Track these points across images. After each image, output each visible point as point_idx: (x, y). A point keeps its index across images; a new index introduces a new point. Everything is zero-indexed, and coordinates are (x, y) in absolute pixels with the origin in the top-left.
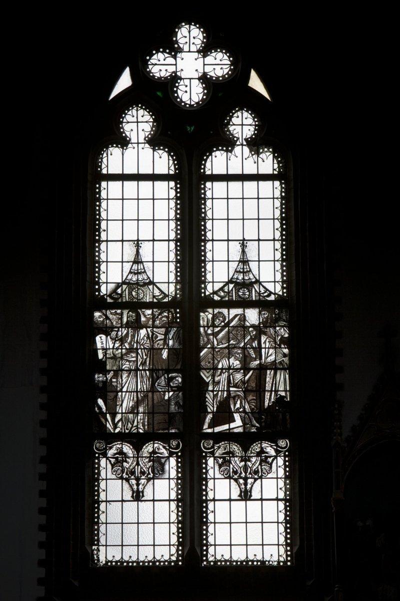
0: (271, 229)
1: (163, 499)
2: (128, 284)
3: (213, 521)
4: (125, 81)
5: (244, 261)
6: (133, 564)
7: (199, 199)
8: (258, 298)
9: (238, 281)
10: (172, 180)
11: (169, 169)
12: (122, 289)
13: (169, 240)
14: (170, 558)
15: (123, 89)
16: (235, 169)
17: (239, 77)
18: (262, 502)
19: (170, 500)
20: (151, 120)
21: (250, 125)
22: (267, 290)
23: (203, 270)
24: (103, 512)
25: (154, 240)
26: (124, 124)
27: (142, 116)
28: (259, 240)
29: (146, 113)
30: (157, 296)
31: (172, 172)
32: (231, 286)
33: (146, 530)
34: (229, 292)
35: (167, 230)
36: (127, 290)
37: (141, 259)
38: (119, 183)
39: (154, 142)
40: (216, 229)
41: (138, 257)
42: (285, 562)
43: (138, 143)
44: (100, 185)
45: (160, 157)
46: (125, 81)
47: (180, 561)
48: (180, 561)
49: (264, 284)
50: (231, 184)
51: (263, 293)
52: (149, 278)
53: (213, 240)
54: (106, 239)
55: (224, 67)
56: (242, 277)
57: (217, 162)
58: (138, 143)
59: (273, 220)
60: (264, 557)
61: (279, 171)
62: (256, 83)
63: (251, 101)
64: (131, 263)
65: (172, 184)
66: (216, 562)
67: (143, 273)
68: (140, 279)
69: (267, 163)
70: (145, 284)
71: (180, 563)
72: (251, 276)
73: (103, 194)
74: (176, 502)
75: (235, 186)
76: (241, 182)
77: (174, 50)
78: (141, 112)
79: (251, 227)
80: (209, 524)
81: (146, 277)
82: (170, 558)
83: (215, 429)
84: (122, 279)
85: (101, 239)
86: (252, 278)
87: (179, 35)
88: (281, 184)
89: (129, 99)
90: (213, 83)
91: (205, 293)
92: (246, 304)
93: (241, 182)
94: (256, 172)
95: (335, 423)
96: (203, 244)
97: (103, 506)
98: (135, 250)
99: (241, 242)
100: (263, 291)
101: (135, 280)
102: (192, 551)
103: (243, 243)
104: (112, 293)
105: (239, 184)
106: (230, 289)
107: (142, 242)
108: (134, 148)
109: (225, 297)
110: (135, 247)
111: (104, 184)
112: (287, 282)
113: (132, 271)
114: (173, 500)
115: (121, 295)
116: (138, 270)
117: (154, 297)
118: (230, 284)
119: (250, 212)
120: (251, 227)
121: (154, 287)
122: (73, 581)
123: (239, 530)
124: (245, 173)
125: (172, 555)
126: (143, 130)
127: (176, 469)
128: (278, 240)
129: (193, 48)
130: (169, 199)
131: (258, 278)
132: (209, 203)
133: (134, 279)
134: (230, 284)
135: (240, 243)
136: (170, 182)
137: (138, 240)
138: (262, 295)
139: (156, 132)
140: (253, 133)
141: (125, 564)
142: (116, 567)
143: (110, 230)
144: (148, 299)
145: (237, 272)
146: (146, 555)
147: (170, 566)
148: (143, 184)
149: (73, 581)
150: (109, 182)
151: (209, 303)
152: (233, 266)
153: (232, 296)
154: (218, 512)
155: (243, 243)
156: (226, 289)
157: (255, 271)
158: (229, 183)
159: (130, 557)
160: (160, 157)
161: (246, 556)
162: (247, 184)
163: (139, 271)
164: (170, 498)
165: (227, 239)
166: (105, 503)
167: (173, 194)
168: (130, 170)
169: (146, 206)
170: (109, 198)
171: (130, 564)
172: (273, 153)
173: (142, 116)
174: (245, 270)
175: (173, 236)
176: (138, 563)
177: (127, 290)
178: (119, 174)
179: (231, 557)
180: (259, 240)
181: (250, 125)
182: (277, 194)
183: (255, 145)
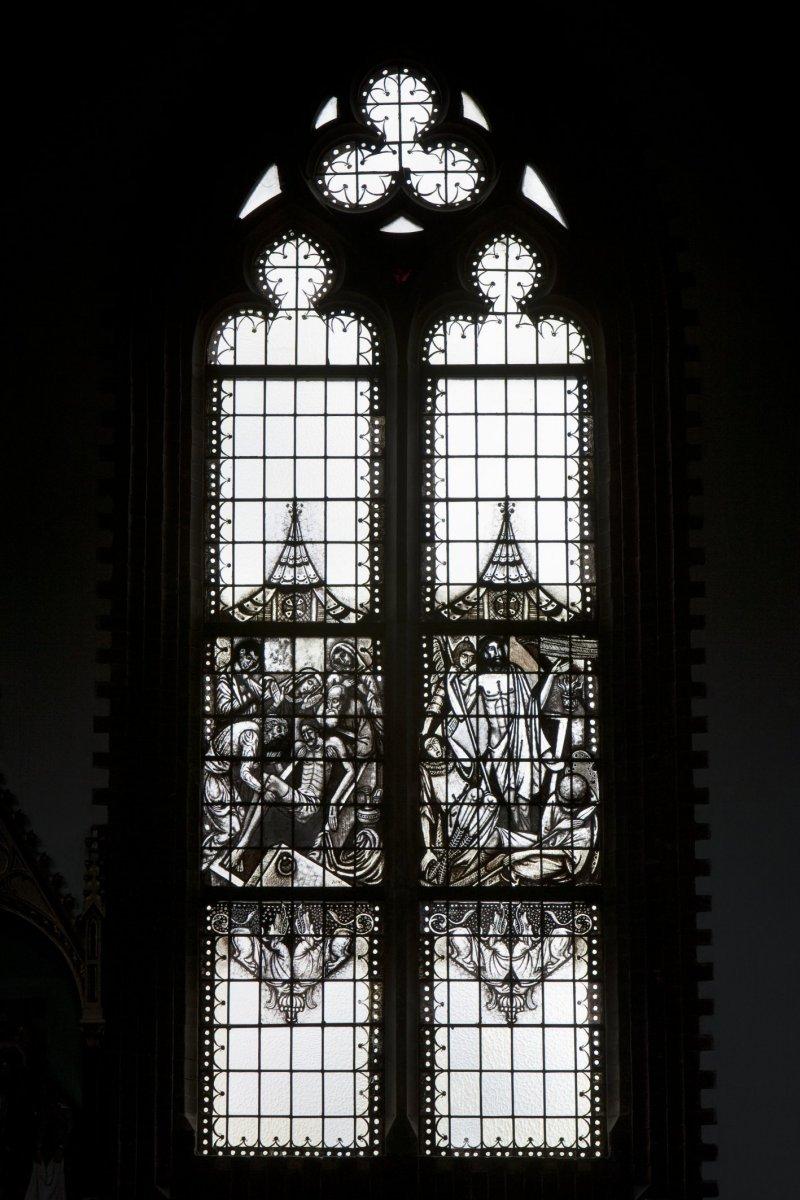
0: (560, 477)
1: (310, 1022)
2: (280, 589)
6: (535, 1154)
8: (321, 618)
9: (284, 583)
11: (569, 353)
12: (264, 597)
13: (233, 500)
14: (355, 1144)
15: (535, 201)
16: (491, 356)
18: (480, 1031)
20: (322, 264)
22: (552, 599)
23: (376, 558)
25: (537, 499)
26: (534, 268)
27: (518, 258)
28: (326, 499)
30: (332, 609)
31: (574, 360)
32: (271, 592)
33: (528, 1085)
34: (265, 605)
35: (352, 479)
37: (513, 535)
40: (452, 477)
41: (507, 527)
42: (590, 1150)
43: (297, 309)
46: (268, 187)
47: (597, 1149)
48: (597, 1149)
49: (545, 587)
50: (272, 385)
51: (546, 606)
53: (566, 499)
55: (360, 158)
56: (292, 574)
57: (453, 343)
58: (297, 309)
60: (325, 1140)
63: (527, 224)
64: (494, 544)
65: (364, 386)
66: (227, 1149)
67: (307, 564)
68: (513, 577)
69: (561, 342)
70: (310, 588)
71: (598, 1154)
72: (523, 571)
74: (368, 1028)
75: (280, 389)
76: (232, 382)
78: (304, 248)
80: (589, 1068)
81: (311, 572)
83: (537, 873)
85: (221, 497)
86: (524, 575)
89: (277, 223)
92: (294, 630)
93: (533, 381)
94: (533, 361)
96: (428, 507)
97: (441, 1036)
98: (500, 516)
99: (503, 502)
100: (544, 603)
101: (290, 578)
102: (402, 1126)
103: (506, 503)
104: (245, 600)
105: (528, 384)
106: (481, 594)
107: (305, 504)
110: (502, 512)
111: (227, 385)
116: (295, 558)
117: (327, 612)
118: (267, 590)
120: (310, 472)
122: (160, 1189)
123: (276, 1085)
124: (542, 361)
125: (581, 1139)
126: (519, 284)
128: (573, 499)
131: (322, 575)
132: (440, 423)
133: (500, 576)
135: (500, 505)
136: (359, 383)
137: (507, 499)
138: (332, 612)
139: (331, 288)
141: (233, 1153)
142: (566, 1161)
143: (238, 478)
145: (282, 564)
147: (355, 1159)
150: (268, 383)
152: (273, 551)
153: (271, 612)
154: (455, 1049)
155: (295, 510)
159: (530, 1140)
163: (298, 562)
166: (446, 1029)
167: (573, 403)
168: (281, 357)
169: (310, 429)
170: (262, 418)
171: (308, 1154)
172: (357, 318)
173: (518, 258)
174: (511, 560)
175: (364, 490)
176: (546, 1150)
178: (562, 365)
179: (259, 1141)
180: (537, 499)
182: (364, 405)
183: (536, 307)
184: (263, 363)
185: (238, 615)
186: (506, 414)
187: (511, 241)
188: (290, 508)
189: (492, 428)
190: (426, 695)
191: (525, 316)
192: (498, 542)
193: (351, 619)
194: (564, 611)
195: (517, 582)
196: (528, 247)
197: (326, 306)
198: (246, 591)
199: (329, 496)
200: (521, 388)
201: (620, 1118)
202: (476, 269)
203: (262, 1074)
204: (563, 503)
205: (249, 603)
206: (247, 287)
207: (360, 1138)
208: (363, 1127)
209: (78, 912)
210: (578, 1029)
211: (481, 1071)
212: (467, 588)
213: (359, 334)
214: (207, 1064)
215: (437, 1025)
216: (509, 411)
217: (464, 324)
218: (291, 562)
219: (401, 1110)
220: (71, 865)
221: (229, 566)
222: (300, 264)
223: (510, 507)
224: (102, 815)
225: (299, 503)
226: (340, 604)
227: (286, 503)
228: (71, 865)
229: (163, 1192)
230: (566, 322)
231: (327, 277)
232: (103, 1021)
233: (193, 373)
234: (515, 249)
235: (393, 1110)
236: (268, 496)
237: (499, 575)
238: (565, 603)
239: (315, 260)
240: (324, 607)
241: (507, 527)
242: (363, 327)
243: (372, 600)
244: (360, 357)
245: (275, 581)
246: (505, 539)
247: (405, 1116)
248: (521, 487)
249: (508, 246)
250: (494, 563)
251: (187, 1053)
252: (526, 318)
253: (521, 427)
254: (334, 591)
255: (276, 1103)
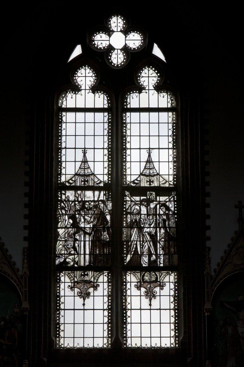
0: (166, 142)
2: (145, 175)
3: (130, 322)
4: (78, 51)
5: (85, 161)
7: (176, 123)
10: (170, 112)
14: (171, 346)
15: (157, 55)
17: (146, 49)
19: (64, 310)
21: (155, 77)
24: (129, 317)
27: (89, 73)
29: (80, 71)
33: (89, 328)
34: (75, 181)
35: (102, 142)
36: (78, 179)
37: (152, 160)
38: (138, 114)
39: (159, 88)
40: (133, 142)
43: (85, 90)
44: (126, 115)
45: (99, 97)
46: (78, 51)
50: (78, 114)
52: (92, 172)
54: (169, 150)
57: (134, 100)
59: (150, 137)
61: (108, 106)
62: (157, 52)
63: (154, 63)
64: (81, 163)
65: (106, 114)
70: (89, 175)
72: (89, 171)
73: (128, 121)
75: (144, 115)
77: (109, 32)
79: (89, 140)
82: (103, 346)
84: (75, 173)
87: (112, 22)
88: (173, 114)
89: (80, 62)
90: (130, 52)
91: (60, 180)
95: (206, 261)
98: (147, 155)
99: (83, 150)
100: (96, 180)
104: (135, 180)
105: (73, 114)
108: (146, 93)
109: (138, 183)
112: (176, 177)
113: (81, 167)
114: (106, 310)
115: (75, 181)
119: (89, 131)
120: (89, 140)
121: (161, 176)
125: (172, 344)
127: (60, 289)
129: (119, 30)
130: (168, 123)
131: (158, 172)
133: (148, 172)
134: (76, 176)
137: (85, 148)
139: (96, 83)
140: (156, 82)
143: (67, 141)
144: (91, 184)
146: (156, 343)
148: (142, 114)
149: (43, 358)
150: (141, 113)
151: (64, 187)
154: (133, 316)
155: (85, 150)
156: (74, 179)
157: (157, 168)
158: (67, 113)
160: (99, 97)
161: (140, 345)
162: (87, 114)
164: (64, 308)
165: (76, 149)
168: (144, 105)
173: (89, 73)
177: (78, 179)
181: (155, 77)
182: (170, 120)
184: (138, 107)
185: (67, 184)
186: (149, 123)
187: (87, 68)
188: (148, 151)
189: (144, 127)
190: (124, 209)
191: (91, 90)
192: (147, 162)
193: (102, 185)
194: (167, 183)
195: (87, 174)
196: (78, 70)
197: (94, 89)
198: (135, 177)
199: (95, 147)
200: (154, 115)
201: (183, 336)
202: (139, 77)
203: (65, 323)
204: (139, 150)
205: (70, 180)
206: (136, 84)
207: (172, 344)
208: (173, 340)
209: (20, 273)
210: (85, 311)
211: (84, 324)
212: (72, 176)
213: (104, 99)
214: (58, 321)
215: (107, 310)
216: (141, 122)
217: (72, 94)
218: (149, 168)
219: (117, 334)
220: (18, 259)
221: (129, 168)
222: (149, 76)
223: (86, 151)
224: (26, 244)
225: (86, 149)
226: (99, 179)
227: (146, 150)
228: (18, 259)
229: (44, 359)
230: (167, 93)
231: (158, 80)
232: (212, 308)
233: (55, 108)
234: (88, 70)
235: (115, 334)
236: (160, 147)
237: (147, 172)
238: (168, 181)
239: (91, 74)
240: (94, 181)
241: (85, 157)
242: (105, 96)
243: (108, 179)
244: (66, 105)
245: (144, 173)
246: (149, 161)
247: (118, 336)
248: (89, 145)
249: (85, 70)
250: (146, 169)
251: (52, 319)
252: (156, 92)
253: (154, 127)
254: (97, 176)
255: (146, 333)
